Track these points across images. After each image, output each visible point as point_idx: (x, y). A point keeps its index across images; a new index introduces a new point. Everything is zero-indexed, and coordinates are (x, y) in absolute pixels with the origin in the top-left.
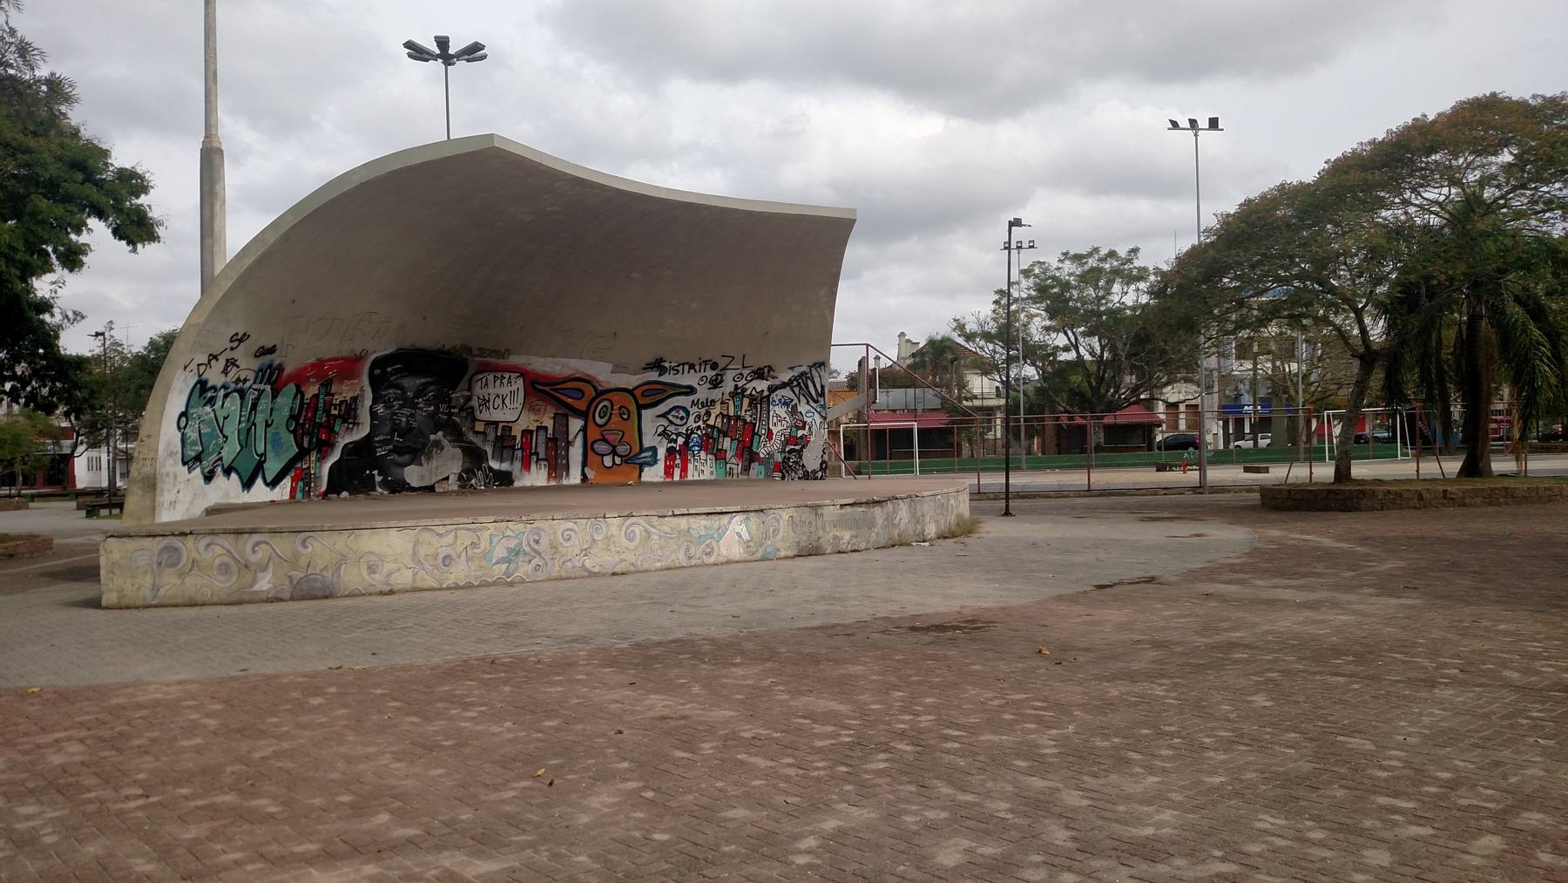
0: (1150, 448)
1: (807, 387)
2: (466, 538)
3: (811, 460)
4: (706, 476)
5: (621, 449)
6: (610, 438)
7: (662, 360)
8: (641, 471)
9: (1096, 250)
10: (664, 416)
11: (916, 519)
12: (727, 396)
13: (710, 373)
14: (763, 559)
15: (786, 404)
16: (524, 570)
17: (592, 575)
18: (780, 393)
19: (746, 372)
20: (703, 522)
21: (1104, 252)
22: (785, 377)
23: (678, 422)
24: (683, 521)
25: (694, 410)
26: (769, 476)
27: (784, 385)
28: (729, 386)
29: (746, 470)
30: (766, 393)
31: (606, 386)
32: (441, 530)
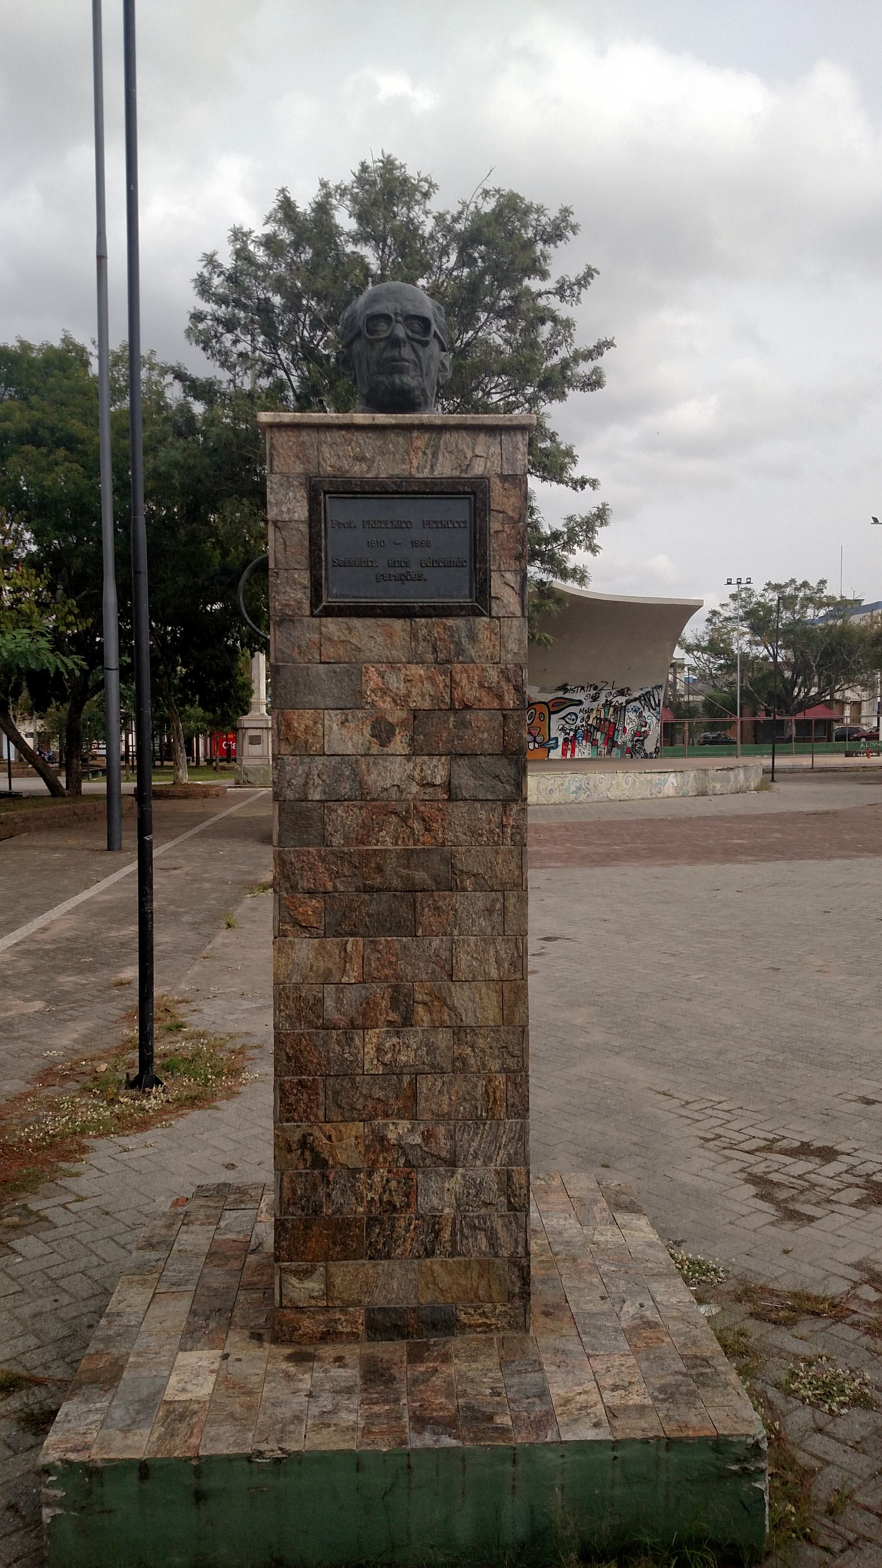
0: (829, 740)
1: (650, 701)
2: (559, 781)
3: (650, 745)
4: (586, 756)
5: (538, 739)
6: (533, 732)
7: (567, 685)
8: (549, 752)
9: (793, 581)
10: (563, 718)
11: (747, 779)
12: (601, 706)
13: (593, 692)
14: (683, 796)
15: (635, 711)
16: (583, 797)
17: (611, 800)
19: (613, 692)
20: (657, 776)
21: (799, 582)
22: (636, 695)
23: (571, 722)
24: (649, 775)
25: (580, 715)
27: (635, 699)
28: (602, 700)
29: (609, 752)
30: (624, 704)
31: (535, 701)
32: (549, 777)
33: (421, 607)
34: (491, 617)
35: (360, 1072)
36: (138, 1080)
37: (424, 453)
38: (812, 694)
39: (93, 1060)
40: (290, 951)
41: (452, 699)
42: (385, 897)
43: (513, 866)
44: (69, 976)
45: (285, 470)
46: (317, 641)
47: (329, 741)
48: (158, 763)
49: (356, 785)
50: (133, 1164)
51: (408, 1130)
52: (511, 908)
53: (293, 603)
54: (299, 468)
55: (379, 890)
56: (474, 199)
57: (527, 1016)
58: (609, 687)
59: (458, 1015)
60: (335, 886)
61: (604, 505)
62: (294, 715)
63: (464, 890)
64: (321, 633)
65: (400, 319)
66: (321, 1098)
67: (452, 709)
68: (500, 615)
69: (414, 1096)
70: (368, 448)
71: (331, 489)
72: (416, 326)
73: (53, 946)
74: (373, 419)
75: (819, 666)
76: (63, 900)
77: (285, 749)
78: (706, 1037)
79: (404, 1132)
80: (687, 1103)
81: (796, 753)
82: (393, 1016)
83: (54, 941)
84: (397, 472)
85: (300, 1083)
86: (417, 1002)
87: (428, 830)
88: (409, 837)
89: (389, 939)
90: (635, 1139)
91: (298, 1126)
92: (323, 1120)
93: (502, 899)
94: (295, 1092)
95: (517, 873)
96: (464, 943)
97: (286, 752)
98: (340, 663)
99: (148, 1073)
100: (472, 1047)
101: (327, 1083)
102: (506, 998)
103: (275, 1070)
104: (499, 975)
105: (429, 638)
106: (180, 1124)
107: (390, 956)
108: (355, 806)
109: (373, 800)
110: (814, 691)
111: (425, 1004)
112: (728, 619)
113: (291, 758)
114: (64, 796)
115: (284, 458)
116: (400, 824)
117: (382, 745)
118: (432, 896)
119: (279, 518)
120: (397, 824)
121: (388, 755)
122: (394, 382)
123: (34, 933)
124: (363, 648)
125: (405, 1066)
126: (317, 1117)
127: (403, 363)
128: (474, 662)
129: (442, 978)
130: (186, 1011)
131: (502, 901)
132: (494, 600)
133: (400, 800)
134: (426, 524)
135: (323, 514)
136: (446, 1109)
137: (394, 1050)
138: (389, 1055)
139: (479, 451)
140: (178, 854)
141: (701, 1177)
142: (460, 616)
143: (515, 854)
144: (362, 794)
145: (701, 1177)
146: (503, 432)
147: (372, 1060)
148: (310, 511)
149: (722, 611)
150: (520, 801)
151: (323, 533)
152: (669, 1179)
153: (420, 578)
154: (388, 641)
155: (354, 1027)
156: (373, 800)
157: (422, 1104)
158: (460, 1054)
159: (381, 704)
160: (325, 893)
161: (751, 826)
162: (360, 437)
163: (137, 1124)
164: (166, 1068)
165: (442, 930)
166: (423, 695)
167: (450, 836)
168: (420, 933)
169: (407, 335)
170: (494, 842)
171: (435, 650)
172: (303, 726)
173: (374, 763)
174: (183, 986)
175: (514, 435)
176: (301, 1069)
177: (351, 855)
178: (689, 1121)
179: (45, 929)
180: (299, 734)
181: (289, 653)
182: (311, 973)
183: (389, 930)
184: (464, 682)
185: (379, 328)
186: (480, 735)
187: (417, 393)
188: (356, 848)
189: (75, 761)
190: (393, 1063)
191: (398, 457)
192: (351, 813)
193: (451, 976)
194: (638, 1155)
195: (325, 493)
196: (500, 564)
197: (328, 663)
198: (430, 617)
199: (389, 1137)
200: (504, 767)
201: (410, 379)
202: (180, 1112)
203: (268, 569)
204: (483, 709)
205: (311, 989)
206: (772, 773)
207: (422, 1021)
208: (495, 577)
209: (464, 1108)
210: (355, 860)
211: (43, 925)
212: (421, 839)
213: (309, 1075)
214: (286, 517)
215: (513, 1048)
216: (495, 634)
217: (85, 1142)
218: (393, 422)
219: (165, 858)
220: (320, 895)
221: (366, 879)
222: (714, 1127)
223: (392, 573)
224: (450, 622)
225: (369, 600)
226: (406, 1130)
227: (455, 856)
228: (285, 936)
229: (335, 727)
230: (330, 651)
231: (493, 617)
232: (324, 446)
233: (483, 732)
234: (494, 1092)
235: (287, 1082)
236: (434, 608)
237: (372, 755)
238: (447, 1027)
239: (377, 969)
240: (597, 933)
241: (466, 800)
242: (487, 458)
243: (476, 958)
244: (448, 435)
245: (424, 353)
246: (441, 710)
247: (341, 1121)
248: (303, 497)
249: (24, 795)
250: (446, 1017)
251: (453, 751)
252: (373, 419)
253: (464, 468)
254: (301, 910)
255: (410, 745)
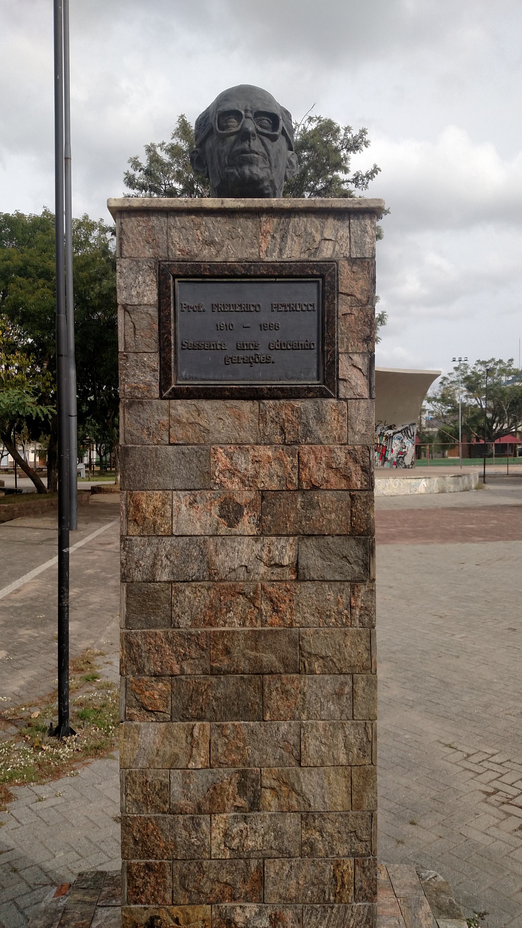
0: (515, 456)
3: (408, 460)
9: (493, 359)
15: (399, 439)
18: (397, 435)
19: (385, 427)
21: (497, 360)
22: (400, 429)
26: (391, 467)
27: (399, 432)
29: (383, 464)
33: (270, 389)
34: (339, 398)
35: (207, 856)
36: (58, 729)
37: (273, 237)
38: (504, 428)
39: (30, 706)
40: (136, 736)
41: (299, 479)
42: (233, 679)
43: (361, 648)
44: (27, 629)
45: (134, 254)
46: (166, 423)
47: (177, 522)
48: (108, 469)
49: (204, 566)
50: (44, 815)
51: (256, 914)
52: (360, 692)
53: (142, 386)
54: (149, 253)
55: (226, 673)
56: (303, 123)
57: (376, 801)
58: (382, 424)
59: (307, 801)
60: (182, 669)
61: (383, 312)
62: (142, 497)
63: (312, 672)
64: (170, 415)
65: (250, 115)
66: (169, 882)
67: (299, 489)
68: (348, 397)
69: (262, 880)
70: (217, 233)
71: (180, 273)
72: (266, 122)
73: (21, 604)
74: (222, 203)
75: (508, 411)
76: (33, 567)
77: (134, 530)
78: (476, 692)
79: (251, 916)
80: (469, 755)
81: (496, 464)
82: (241, 802)
83: (22, 600)
84: (245, 256)
85: (148, 866)
86: (265, 788)
87: (276, 610)
88: (256, 618)
89: (236, 723)
90: (433, 794)
91: (145, 909)
92: (170, 901)
93: (350, 683)
94: (142, 874)
95: (366, 655)
96: (312, 728)
97: (135, 533)
98: (189, 444)
99: (65, 726)
100: (320, 831)
101: (174, 867)
102: (355, 783)
103: (123, 853)
104: (348, 760)
105: (277, 420)
106: (84, 772)
107: (238, 741)
108: (203, 587)
109: (221, 580)
110: (506, 426)
111: (273, 789)
112: (452, 382)
113: (139, 539)
114: (46, 493)
115: (133, 242)
116: (248, 604)
117: (230, 525)
118: (280, 679)
119: (129, 302)
120: (245, 605)
121: (236, 535)
122: (244, 173)
123: (11, 593)
124: (212, 429)
125: (252, 851)
126: (164, 900)
127: (252, 155)
128: (322, 443)
129: (291, 763)
130: (101, 663)
131: (351, 684)
132: (341, 382)
133: (248, 580)
134: (275, 308)
135: (172, 297)
136: (294, 894)
137: (241, 836)
138: (237, 841)
139: (328, 234)
140: (113, 533)
141: (490, 836)
142: (309, 398)
143: (363, 636)
144: (210, 574)
145: (490, 836)
146: (352, 216)
147: (219, 845)
148: (159, 295)
149: (449, 377)
150: (368, 582)
151: (172, 317)
152: (464, 838)
153: (268, 361)
154: (237, 423)
155: (200, 812)
156: (221, 580)
157: (270, 888)
158: (308, 839)
159: (230, 485)
160: (172, 676)
161: (476, 515)
162: (209, 221)
163: (52, 773)
164: (82, 717)
165: (290, 714)
166: (271, 476)
167: (298, 617)
168: (267, 718)
169: (257, 130)
170: (343, 624)
171: (283, 431)
172: (151, 507)
173: (222, 544)
174: (102, 640)
175: (363, 218)
176: (148, 853)
177: (198, 636)
178: (472, 775)
179: (18, 590)
180: (147, 515)
181: (138, 435)
182: (157, 758)
183: (236, 714)
184: (312, 463)
185: (229, 124)
186: (328, 516)
187: (266, 184)
188: (203, 630)
189: (53, 471)
190: (240, 849)
191: (246, 240)
192: (199, 594)
193: (299, 761)
194: (437, 811)
195: (175, 277)
196: (347, 346)
197: (176, 445)
198: (278, 398)
199: (237, 920)
200: (351, 547)
201: (259, 170)
202: (86, 761)
203: (118, 352)
204: (331, 490)
205: (157, 775)
206: (483, 477)
207: (270, 805)
208: (343, 358)
209: (312, 892)
210: (203, 642)
211: (18, 587)
212: (269, 620)
213: (156, 859)
214: (135, 301)
215: (362, 832)
216: (343, 416)
217: (12, 790)
218: (242, 205)
219: (104, 536)
220: (167, 678)
221: (213, 661)
222: (492, 781)
223: (241, 356)
224: (298, 404)
225: (218, 383)
226: (253, 913)
227: (303, 638)
228: (131, 720)
229: (184, 508)
230: (178, 433)
231: (341, 399)
232: (174, 231)
233: (331, 513)
234: (342, 876)
235: (134, 864)
236: (282, 390)
237: (221, 536)
238: (295, 812)
239: (224, 754)
240: (386, 597)
241: (314, 580)
242: (336, 241)
243: (325, 744)
244: (296, 219)
245: (273, 147)
246: (288, 490)
247: (189, 904)
248: (152, 280)
249: (24, 491)
250: (294, 803)
251: (301, 531)
252: (222, 203)
253: (313, 251)
254: (147, 693)
255: (258, 526)
